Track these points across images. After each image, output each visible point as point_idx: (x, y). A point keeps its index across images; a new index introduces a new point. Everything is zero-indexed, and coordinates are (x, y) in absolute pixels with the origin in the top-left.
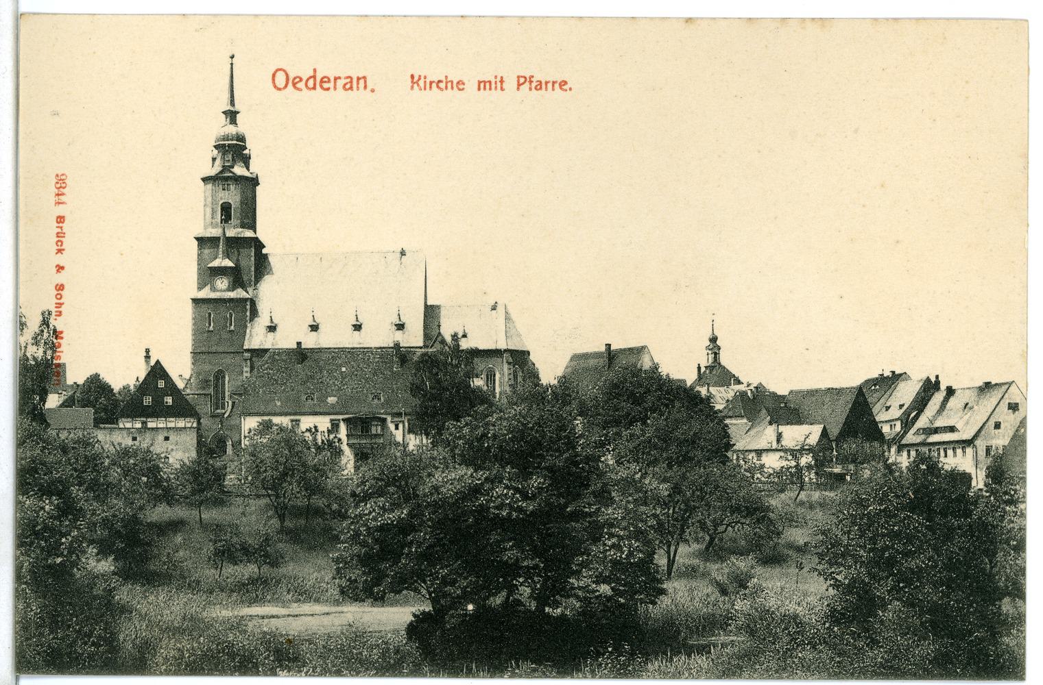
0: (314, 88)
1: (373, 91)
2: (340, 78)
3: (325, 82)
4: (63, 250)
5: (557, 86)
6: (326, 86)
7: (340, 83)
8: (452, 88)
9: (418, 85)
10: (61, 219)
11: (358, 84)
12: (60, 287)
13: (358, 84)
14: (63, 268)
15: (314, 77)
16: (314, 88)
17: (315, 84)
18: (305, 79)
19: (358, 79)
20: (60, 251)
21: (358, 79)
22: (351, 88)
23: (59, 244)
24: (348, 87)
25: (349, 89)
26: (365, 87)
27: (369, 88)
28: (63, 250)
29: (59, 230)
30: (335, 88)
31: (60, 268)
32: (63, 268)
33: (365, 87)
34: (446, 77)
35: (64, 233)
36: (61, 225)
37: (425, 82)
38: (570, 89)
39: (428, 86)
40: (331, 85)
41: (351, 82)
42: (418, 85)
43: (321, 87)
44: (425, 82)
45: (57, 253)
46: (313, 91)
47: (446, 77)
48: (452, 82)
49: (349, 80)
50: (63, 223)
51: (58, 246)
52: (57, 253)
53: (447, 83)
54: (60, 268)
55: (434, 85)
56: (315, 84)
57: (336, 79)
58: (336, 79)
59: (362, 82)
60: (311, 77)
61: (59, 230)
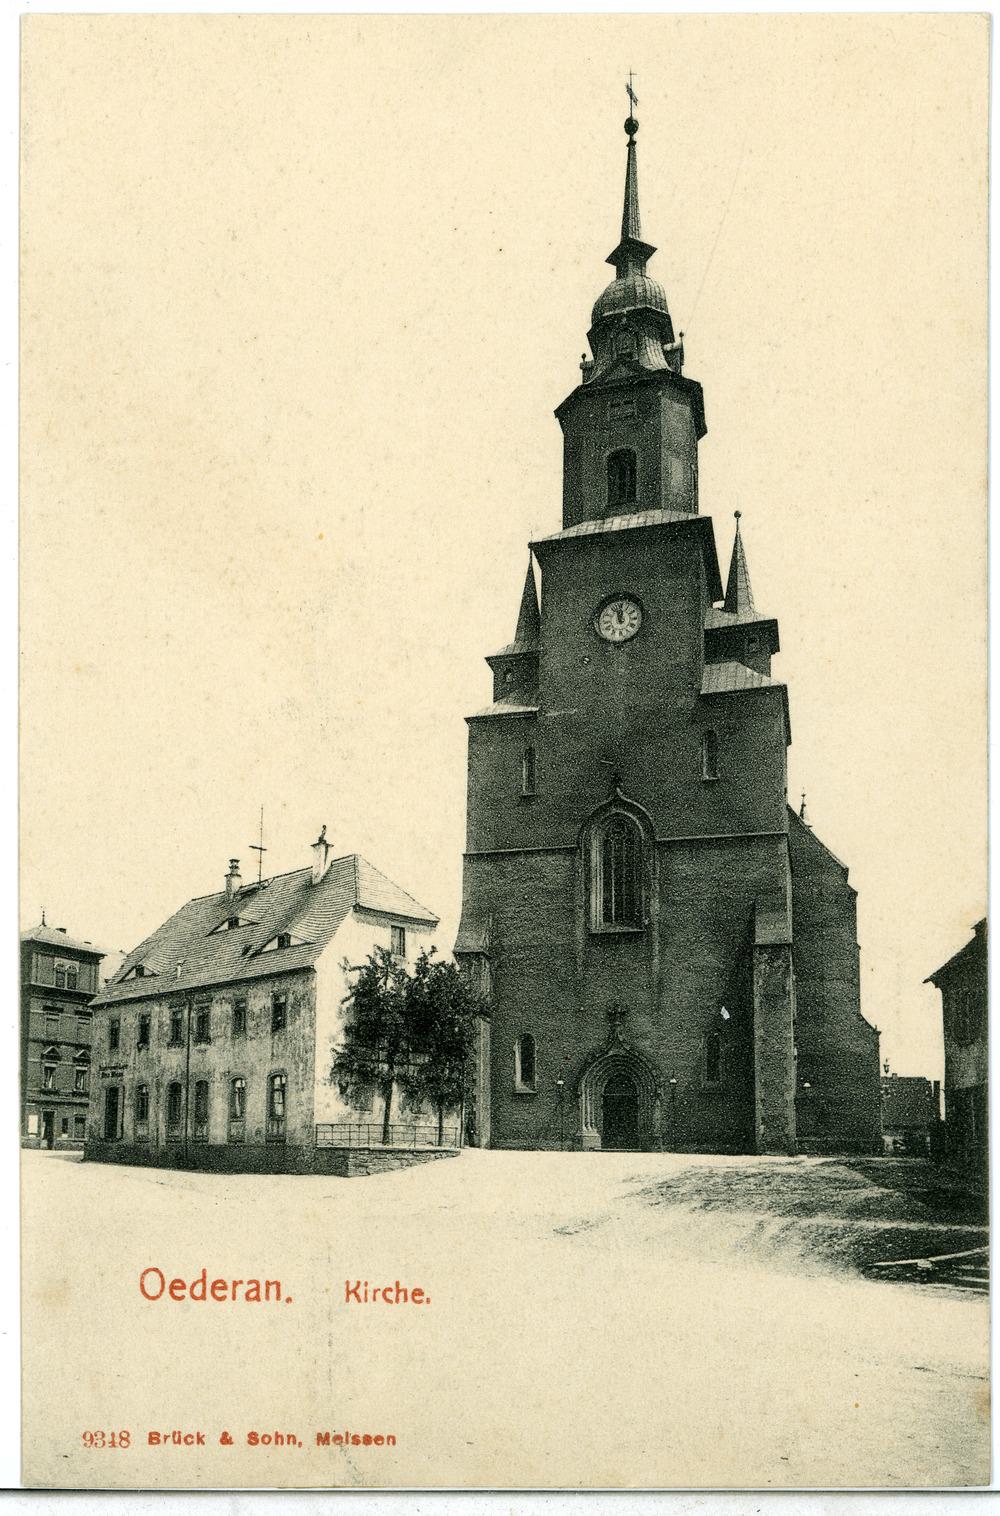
0: (203, 1297)
1: (289, 1300)
2: (241, 1282)
3: (252, 1290)
4: (198, 1434)
5: (379, 1294)
6: (219, 1293)
7: (241, 1290)
8: (406, 1299)
9: (357, 1296)
10: (154, 1438)
11: (267, 1291)
12: (253, 1438)
13: (267, 1291)
14: (225, 1434)
15: (203, 1280)
16: (203, 1297)
17: (204, 1291)
18: (189, 1285)
19: (268, 1284)
20: (200, 1440)
21: (268, 1284)
22: (257, 1298)
23: (189, 1440)
24: (254, 1296)
25: (254, 1299)
26: (278, 1297)
27: (283, 1297)
28: (198, 1434)
29: (170, 1440)
30: (234, 1298)
31: (226, 1440)
32: (225, 1434)
33: (278, 1297)
34: (397, 1284)
35: (174, 1433)
36: (162, 1439)
37: (366, 1293)
38: (428, 1301)
39: (370, 1295)
40: (228, 1293)
41: (257, 1289)
42: (357, 1296)
43: (214, 1295)
44: (366, 1293)
45: (203, 1443)
46: (201, 1302)
47: (397, 1284)
48: (405, 1291)
49: (253, 1286)
50: (158, 1434)
51: (192, 1442)
52: (203, 1443)
53: (398, 1291)
54: (226, 1440)
55: (379, 1294)
56: (204, 1291)
57: (235, 1284)
58: (235, 1284)
59: (273, 1289)
60: (198, 1282)
61: (170, 1440)
